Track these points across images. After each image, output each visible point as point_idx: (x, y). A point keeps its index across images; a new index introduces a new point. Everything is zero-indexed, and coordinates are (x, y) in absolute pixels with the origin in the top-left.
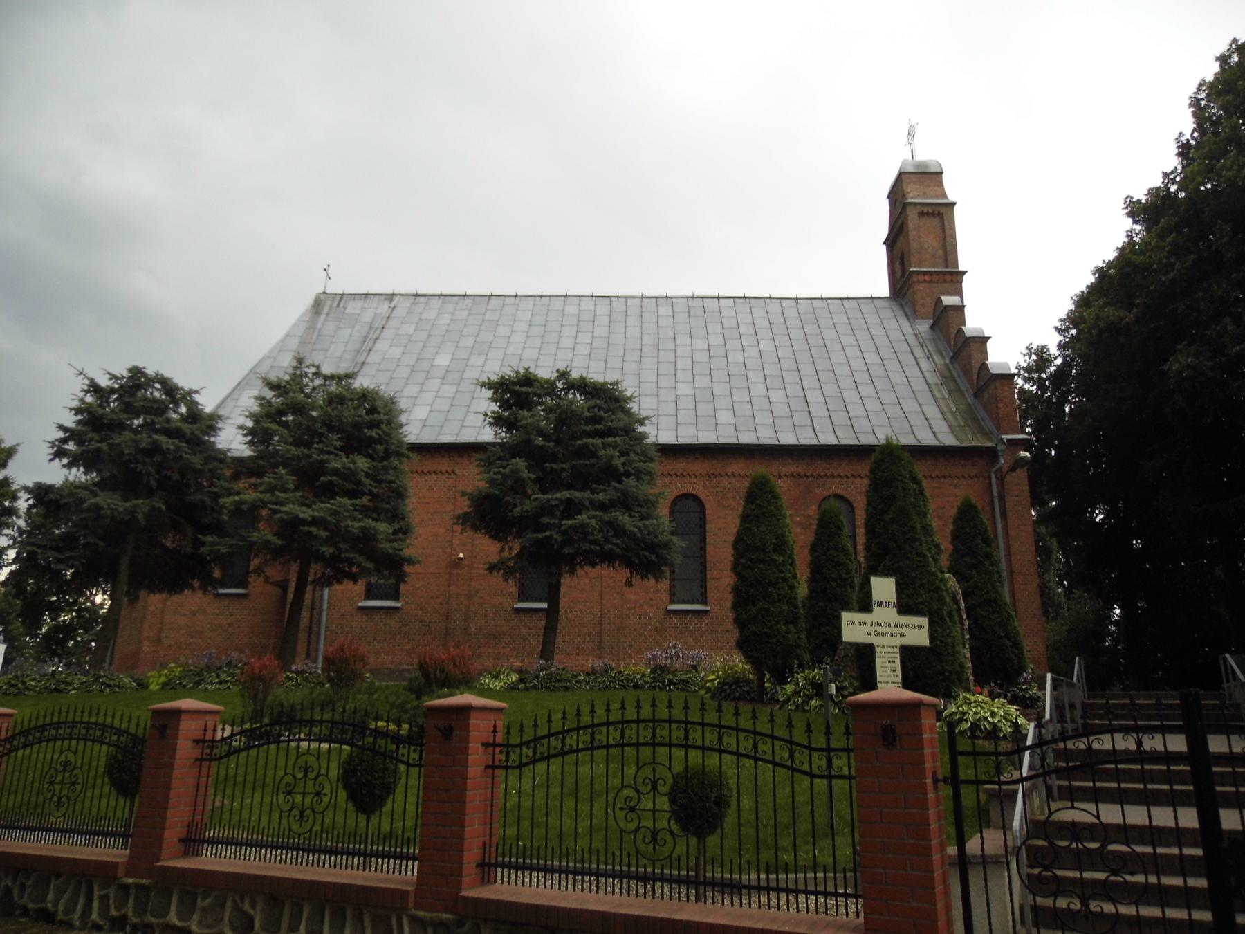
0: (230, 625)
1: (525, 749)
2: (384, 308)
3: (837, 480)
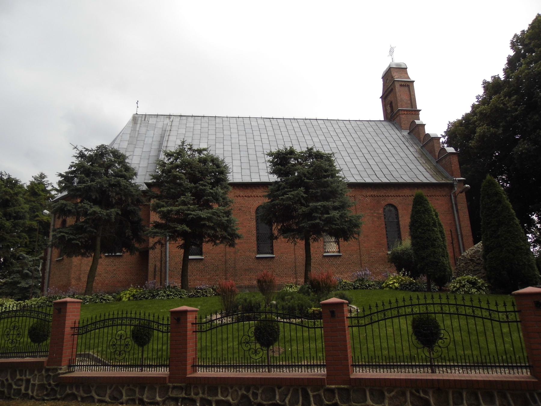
0: (114, 270)
1: (379, 315)
2: (167, 121)
3: (390, 198)
